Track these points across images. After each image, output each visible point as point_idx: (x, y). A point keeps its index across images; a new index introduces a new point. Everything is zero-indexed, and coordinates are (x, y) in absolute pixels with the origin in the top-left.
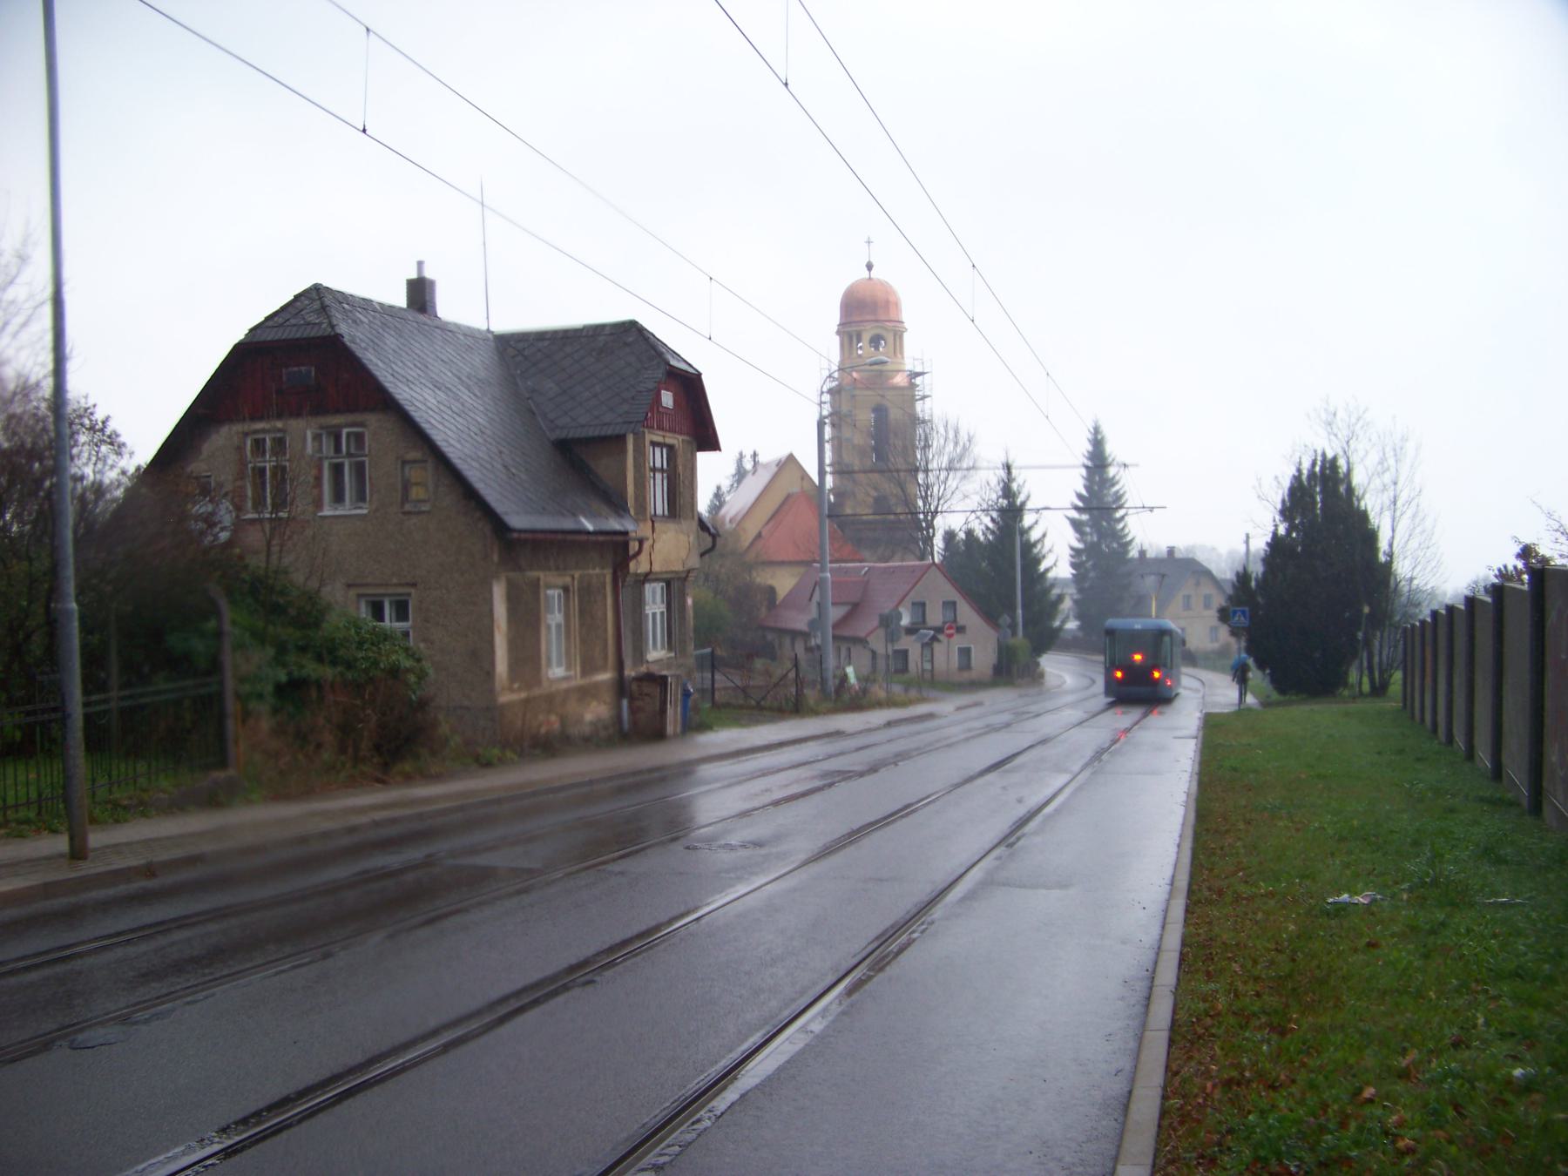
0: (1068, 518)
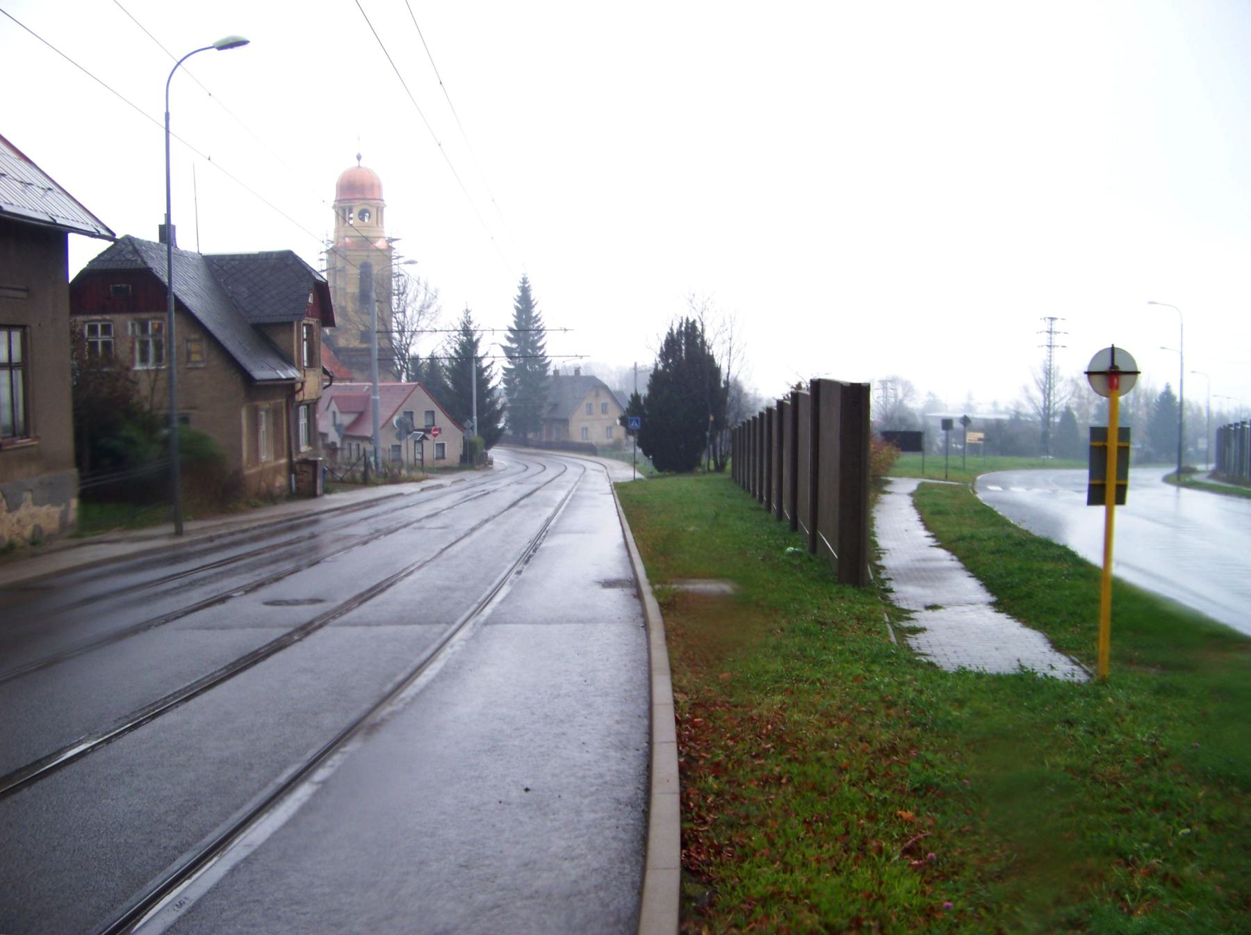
0: (503, 347)
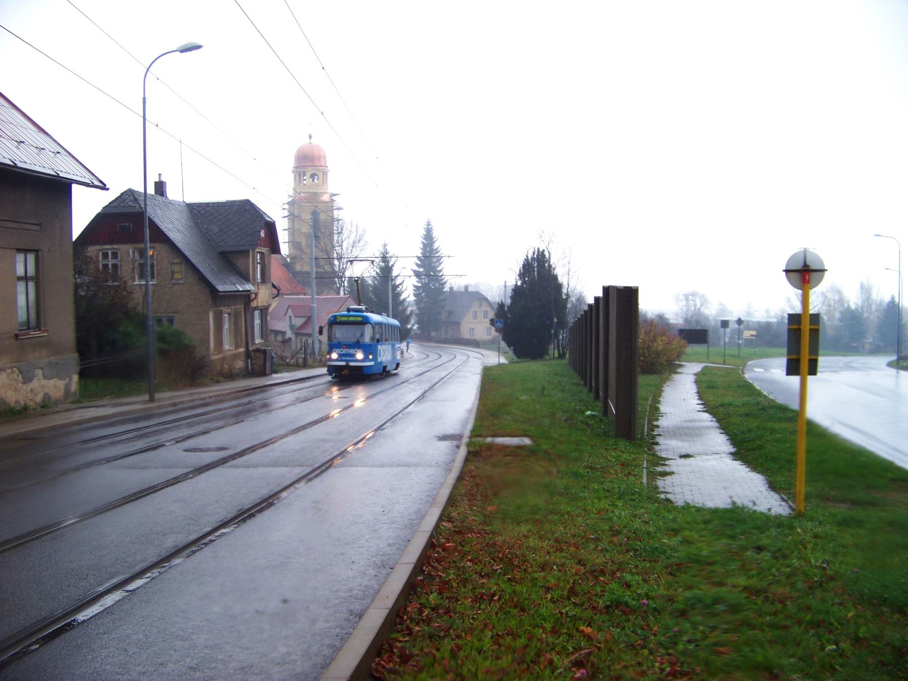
0: (413, 270)
